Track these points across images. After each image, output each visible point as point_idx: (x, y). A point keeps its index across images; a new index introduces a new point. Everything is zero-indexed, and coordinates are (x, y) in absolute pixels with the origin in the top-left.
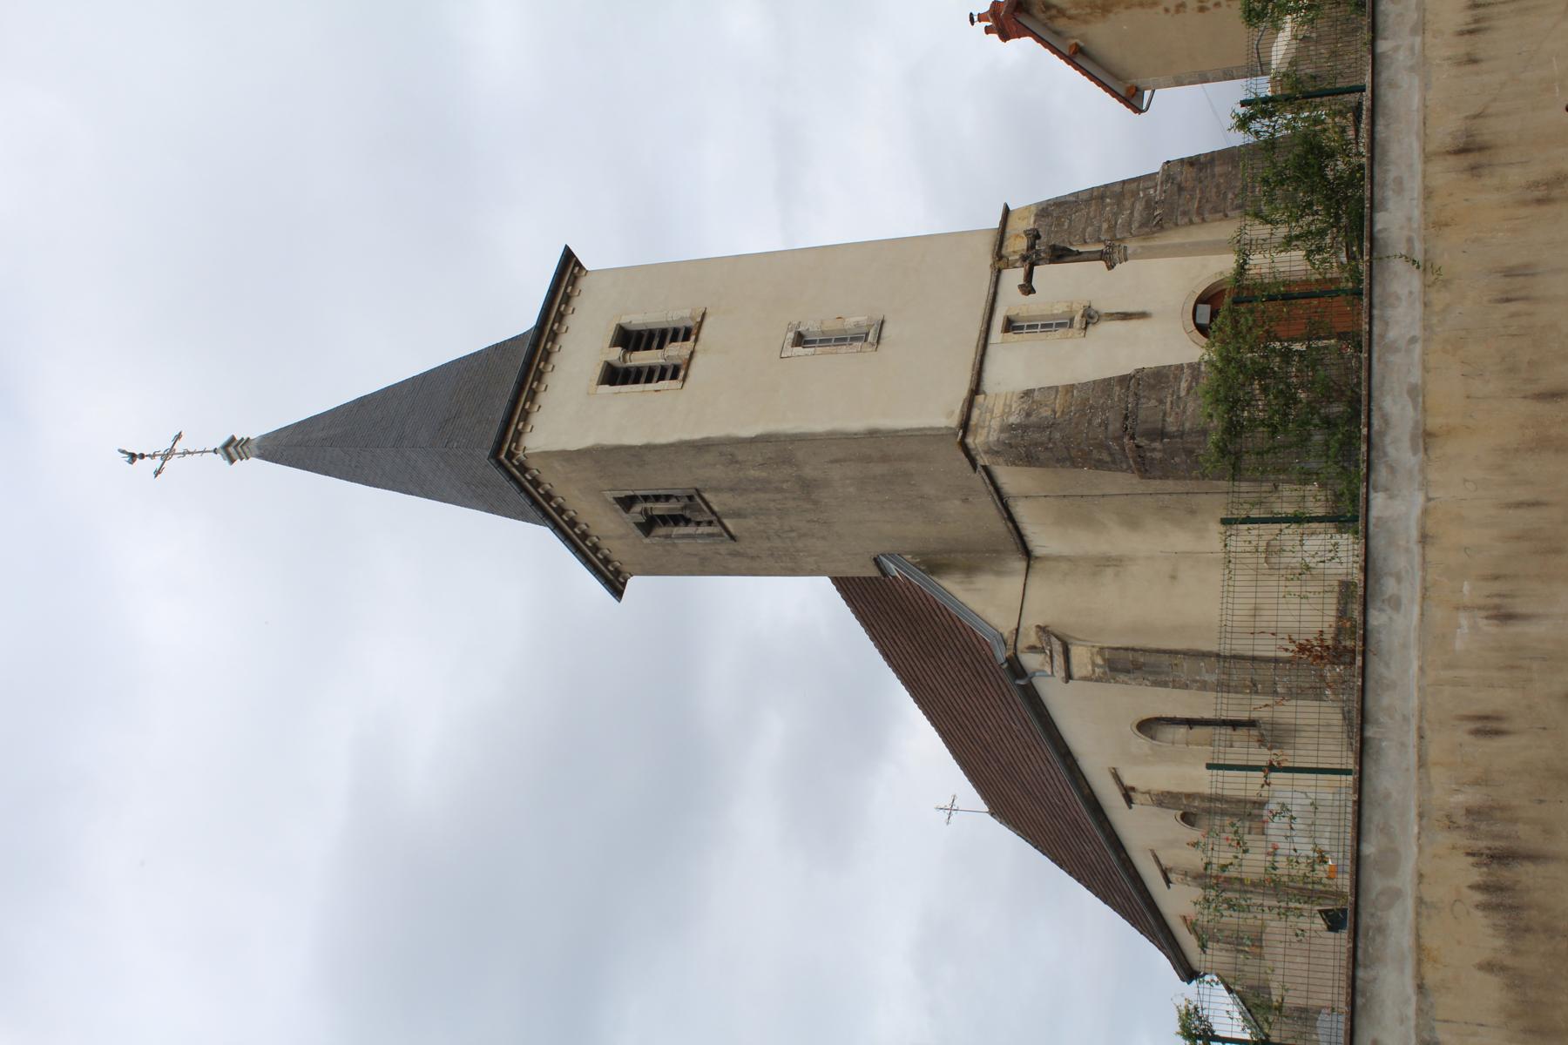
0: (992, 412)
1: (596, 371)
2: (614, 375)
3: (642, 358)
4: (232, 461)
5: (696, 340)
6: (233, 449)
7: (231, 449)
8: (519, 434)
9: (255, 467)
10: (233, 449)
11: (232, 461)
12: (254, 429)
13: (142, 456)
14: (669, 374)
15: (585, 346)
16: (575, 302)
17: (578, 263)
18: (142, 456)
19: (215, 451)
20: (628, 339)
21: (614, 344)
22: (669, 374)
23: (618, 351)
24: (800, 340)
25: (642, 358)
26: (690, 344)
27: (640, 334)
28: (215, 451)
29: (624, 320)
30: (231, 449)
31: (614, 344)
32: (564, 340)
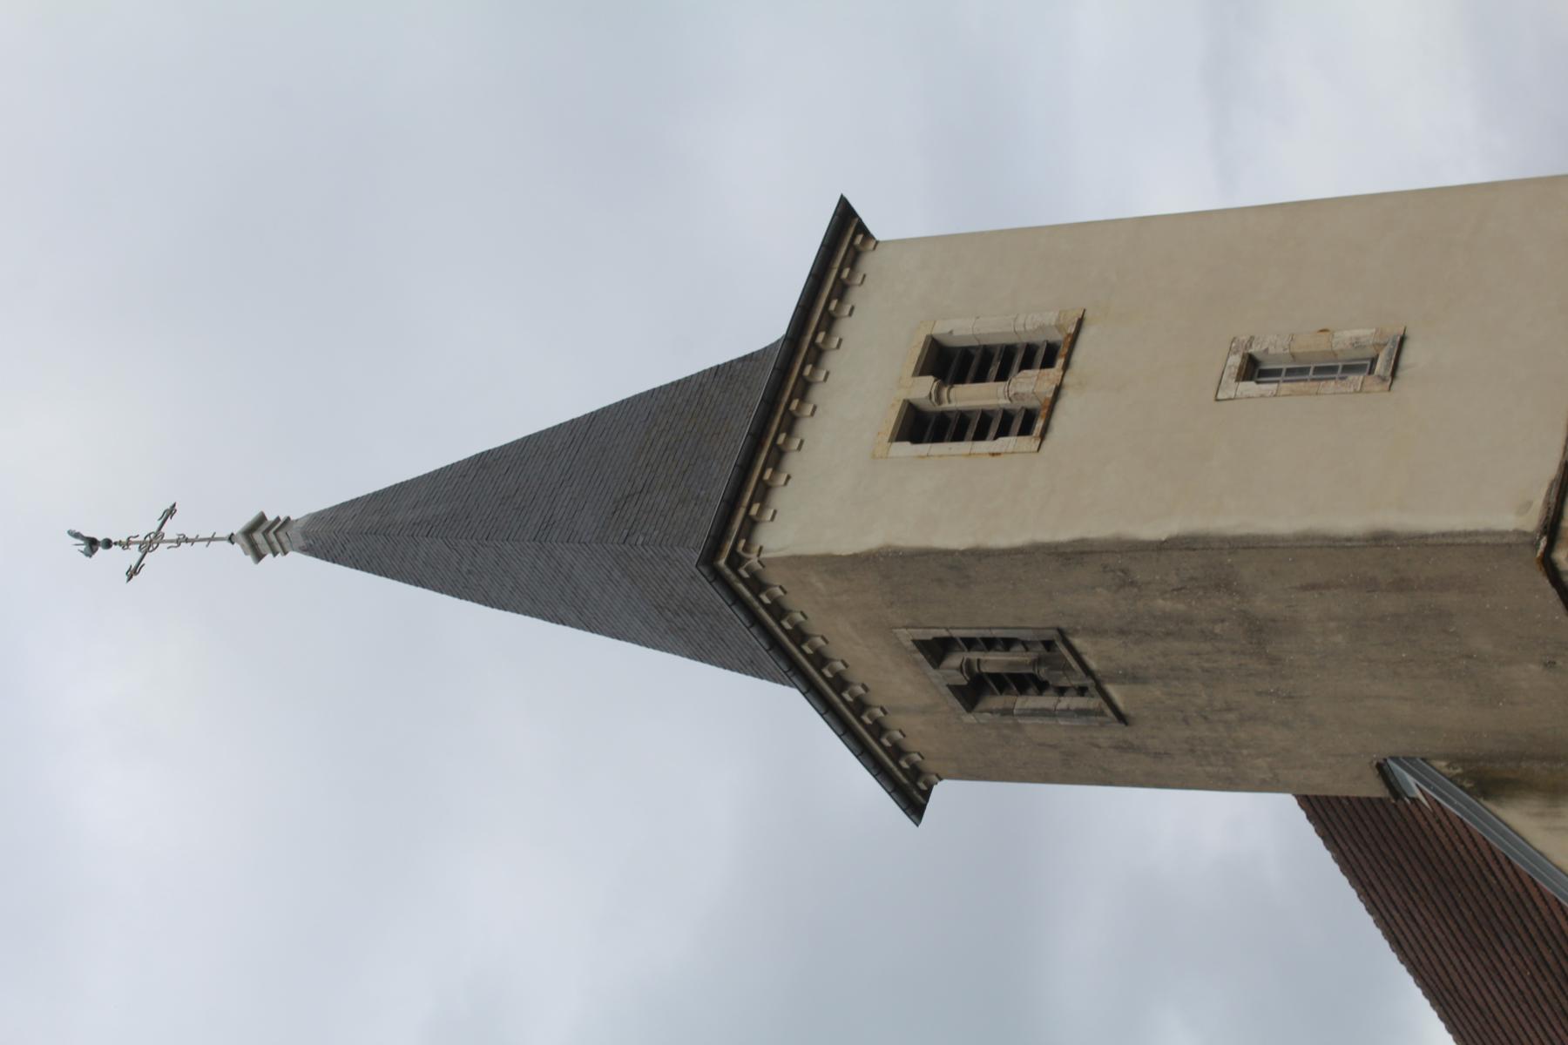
1: (889, 418)
2: (919, 426)
3: (970, 396)
4: (259, 557)
5: (1066, 366)
6: (261, 537)
7: (258, 537)
8: (751, 524)
9: (297, 566)
10: (261, 537)
11: (259, 557)
12: (300, 501)
13: (108, 544)
14: (1016, 425)
15: (870, 373)
16: (855, 296)
17: (862, 229)
18: (108, 544)
19: (231, 539)
20: (947, 361)
21: (922, 370)
22: (1016, 425)
23: (928, 382)
24: (1252, 369)
25: (970, 396)
26: (1054, 373)
27: (966, 353)
28: (231, 539)
29: (940, 329)
30: (258, 537)
31: (922, 370)
32: (834, 361)
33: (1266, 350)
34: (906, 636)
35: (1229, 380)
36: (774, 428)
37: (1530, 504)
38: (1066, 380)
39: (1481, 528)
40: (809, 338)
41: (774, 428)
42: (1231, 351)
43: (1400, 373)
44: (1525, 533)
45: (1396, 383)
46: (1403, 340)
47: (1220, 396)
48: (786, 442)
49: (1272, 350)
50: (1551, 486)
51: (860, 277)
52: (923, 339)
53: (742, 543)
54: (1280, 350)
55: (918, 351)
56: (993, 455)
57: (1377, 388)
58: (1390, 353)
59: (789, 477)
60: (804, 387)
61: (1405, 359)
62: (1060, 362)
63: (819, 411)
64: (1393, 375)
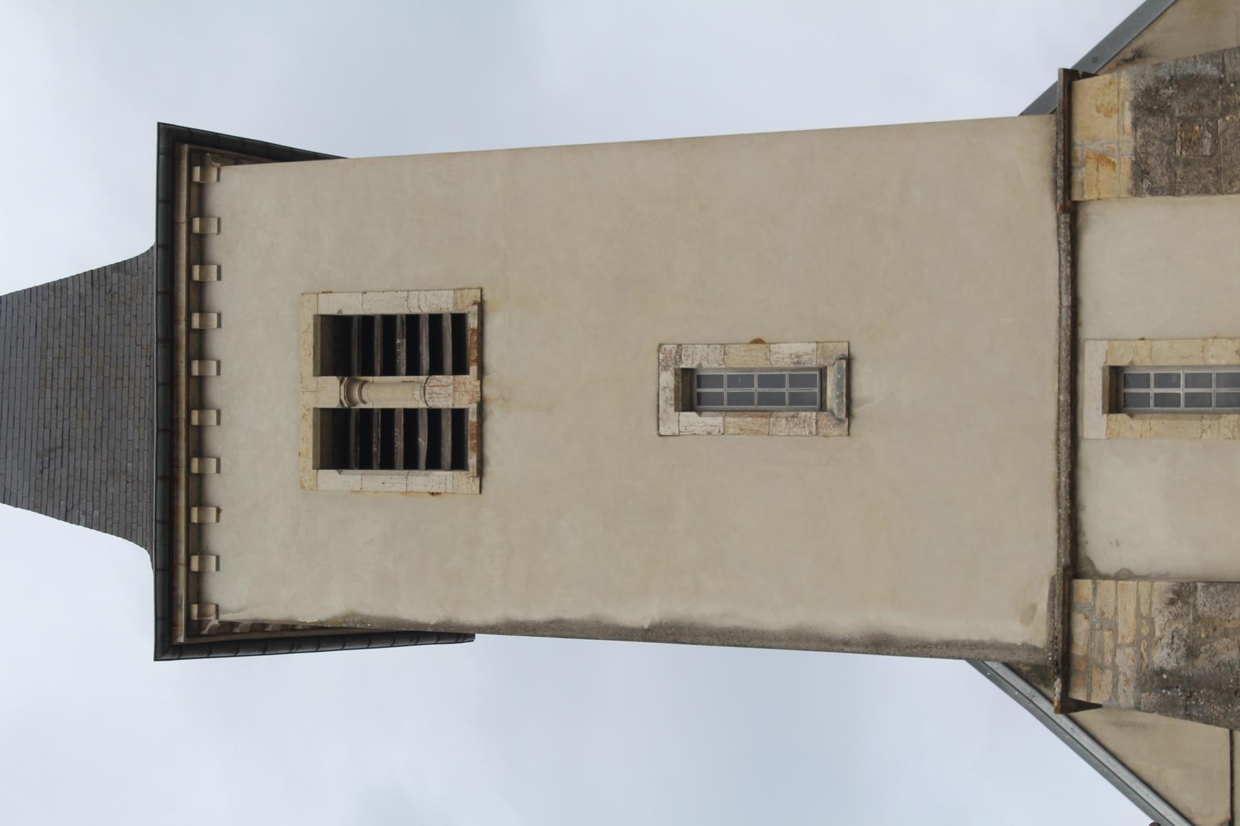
0: (1114, 629)
8: (197, 581)
16: (218, 248)
20: (350, 344)
24: (692, 391)
32: (221, 343)
33: (700, 365)
34: (1124, 194)
35: (668, 409)
36: (183, 456)
37: (1033, 608)
38: (487, 392)
39: (986, 638)
40: (183, 326)
41: (183, 456)
42: (662, 367)
43: (856, 411)
44: (1035, 649)
45: (854, 424)
46: (849, 360)
47: (662, 432)
48: (201, 465)
49: (705, 365)
50: (1053, 584)
51: (214, 223)
52: (311, 321)
53: (195, 608)
54: (715, 365)
55: (310, 338)
56: (432, 494)
57: (836, 432)
58: (839, 387)
59: (219, 511)
60: (199, 301)
61: (859, 392)
62: (473, 369)
63: (224, 417)
64: (849, 414)
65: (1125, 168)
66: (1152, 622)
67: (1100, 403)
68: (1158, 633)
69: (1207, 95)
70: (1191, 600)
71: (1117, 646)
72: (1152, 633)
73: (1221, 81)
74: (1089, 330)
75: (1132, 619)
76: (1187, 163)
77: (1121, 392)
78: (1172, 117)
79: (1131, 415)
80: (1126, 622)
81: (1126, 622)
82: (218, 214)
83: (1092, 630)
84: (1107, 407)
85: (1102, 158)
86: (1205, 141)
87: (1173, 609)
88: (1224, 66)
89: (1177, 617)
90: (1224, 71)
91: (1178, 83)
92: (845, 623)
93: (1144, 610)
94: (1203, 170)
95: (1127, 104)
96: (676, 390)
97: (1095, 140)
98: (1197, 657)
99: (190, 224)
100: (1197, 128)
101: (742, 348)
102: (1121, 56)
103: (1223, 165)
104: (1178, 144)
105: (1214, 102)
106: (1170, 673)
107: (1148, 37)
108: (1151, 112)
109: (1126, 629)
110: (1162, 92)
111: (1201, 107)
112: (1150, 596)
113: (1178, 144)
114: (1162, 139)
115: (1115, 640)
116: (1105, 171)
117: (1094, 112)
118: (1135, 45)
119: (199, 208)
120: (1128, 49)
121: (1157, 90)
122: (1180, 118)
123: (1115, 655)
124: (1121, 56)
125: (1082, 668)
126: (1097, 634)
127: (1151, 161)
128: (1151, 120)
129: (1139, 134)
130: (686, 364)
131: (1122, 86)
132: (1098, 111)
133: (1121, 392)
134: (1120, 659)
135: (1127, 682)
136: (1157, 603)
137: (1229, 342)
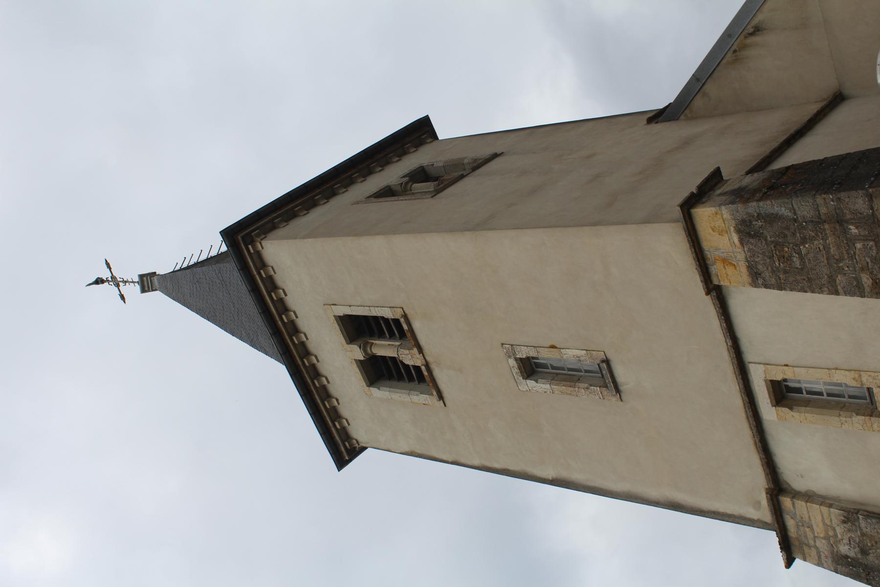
0: (810, 527)
10: (147, 282)
24: (530, 368)
37: (759, 503)
38: (428, 358)
43: (621, 388)
45: (622, 395)
48: (340, 423)
65: (743, 269)
66: (834, 530)
67: (769, 401)
68: (839, 536)
69: (788, 228)
70: (857, 524)
71: (815, 537)
72: (836, 536)
73: (795, 220)
74: (749, 356)
75: (821, 525)
76: (785, 272)
77: (783, 393)
78: (766, 240)
79: (791, 408)
80: (818, 526)
81: (818, 526)
82: (271, 264)
83: (797, 526)
84: (774, 402)
85: (725, 261)
86: (795, 259)
87: (845, 525)
88: (794, 210)
89: (849, 530)
90: (795, 214)
91: (763, 218)
92: (653, 493)
93: (828, 522)
94: (798, 278)
95: (732, 229)
96: (519, 368)
97: (717, 249)
98: (868, 554)
99: (259, 274)
100: (786, 249)
101: (546, 350)
102: (746, 31)
103: (811, 276)
104: (776, 258)
105: (794, 234)
106: (852, 559)
107: (760, 17)
108: (749, 235)
109: (819, 530)
110: (754, 223)
111: (785, 236)
112: (830, 515)
113: (776, 258)
114: (763, 253)
115: (814, 533)
116: (730, 270)
117: (711, 231)
118: (753, 23)
119: (262, 264)
120: (749, 26)
121: (751, 222)
122: (772, 242)
123: (815, 542)
124: (746, 31)
125: (797, 543)
126: (802, 528)
127: (760, 267)
128: (752, 240)
129: (746, 249)
130: (523, 353)
131: (725, 216)
132: (714, 231)
133: (783, 393)
134: (818, 544)
135: (826, 557)
136: (835, 522)
137: (847, 373)
